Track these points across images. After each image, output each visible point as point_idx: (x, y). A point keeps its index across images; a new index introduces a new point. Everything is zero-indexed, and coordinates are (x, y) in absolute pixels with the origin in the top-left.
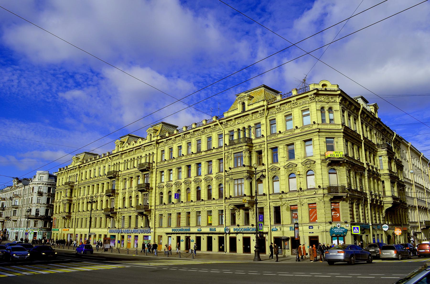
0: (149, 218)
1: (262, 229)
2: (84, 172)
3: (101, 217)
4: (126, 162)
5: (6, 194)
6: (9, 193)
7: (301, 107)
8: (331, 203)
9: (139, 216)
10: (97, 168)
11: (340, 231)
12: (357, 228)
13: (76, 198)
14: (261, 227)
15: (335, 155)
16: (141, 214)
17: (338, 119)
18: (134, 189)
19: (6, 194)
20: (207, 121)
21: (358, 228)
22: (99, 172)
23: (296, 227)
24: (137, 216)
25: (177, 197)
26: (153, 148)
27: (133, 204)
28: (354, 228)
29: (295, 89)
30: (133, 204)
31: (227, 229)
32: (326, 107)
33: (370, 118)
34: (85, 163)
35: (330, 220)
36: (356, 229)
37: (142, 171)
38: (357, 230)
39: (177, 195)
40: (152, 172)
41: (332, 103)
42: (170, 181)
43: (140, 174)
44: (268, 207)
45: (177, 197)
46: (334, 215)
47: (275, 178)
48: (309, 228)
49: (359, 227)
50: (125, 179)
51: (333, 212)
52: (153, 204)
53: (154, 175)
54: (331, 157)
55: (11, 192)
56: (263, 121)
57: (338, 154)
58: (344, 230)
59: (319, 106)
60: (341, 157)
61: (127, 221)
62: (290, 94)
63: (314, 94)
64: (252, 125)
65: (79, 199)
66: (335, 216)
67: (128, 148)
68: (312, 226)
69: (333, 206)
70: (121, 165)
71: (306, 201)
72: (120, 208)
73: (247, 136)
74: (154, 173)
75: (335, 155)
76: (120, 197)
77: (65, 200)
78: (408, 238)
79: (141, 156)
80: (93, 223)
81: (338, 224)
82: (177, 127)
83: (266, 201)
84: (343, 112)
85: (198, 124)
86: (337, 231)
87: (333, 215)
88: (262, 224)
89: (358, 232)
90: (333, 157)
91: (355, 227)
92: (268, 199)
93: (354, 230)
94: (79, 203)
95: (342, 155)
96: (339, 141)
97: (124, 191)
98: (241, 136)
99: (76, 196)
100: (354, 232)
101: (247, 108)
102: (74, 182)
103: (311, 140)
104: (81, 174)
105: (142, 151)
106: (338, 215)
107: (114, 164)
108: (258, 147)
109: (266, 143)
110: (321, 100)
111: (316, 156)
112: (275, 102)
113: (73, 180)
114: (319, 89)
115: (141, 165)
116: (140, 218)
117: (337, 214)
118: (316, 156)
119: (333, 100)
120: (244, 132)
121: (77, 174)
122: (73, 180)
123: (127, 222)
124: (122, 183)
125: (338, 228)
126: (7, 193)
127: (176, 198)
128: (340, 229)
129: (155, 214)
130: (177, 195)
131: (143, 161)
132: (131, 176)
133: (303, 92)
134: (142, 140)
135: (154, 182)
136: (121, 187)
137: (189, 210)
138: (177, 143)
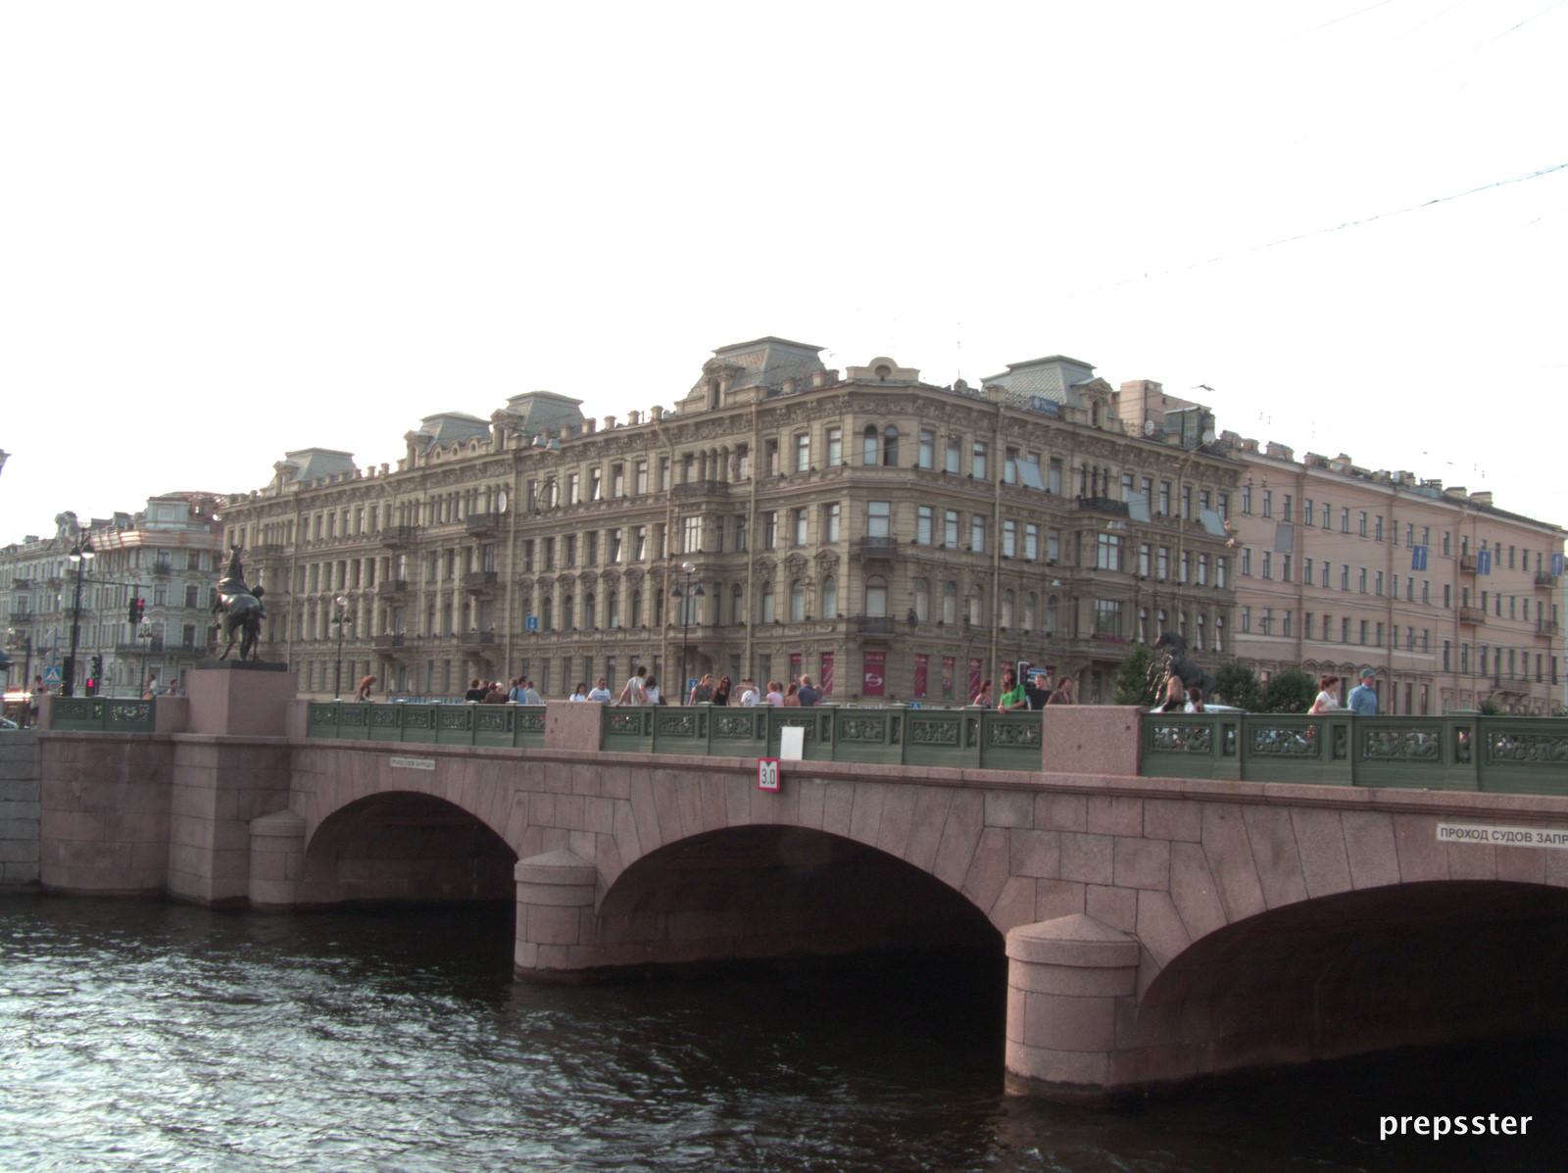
2: (312, 515)
3: (352, 659)
4: (434, 503)
5: (32, 568)
6: (43, 561)
7: (827, 420)
8: (865, 653)
10: (353, 507)
13: (290, 598)
16: (473, 656)
18: (457, 583)
19: (32, 568)
22: (358, 520)
26: (508, 470)
27: (456, 627)
30: (456, 627)
33: (127, 742)
34: (328, 487)
35: (859, 690)
37: (478, 535)
40: (505, 540)
43: (474, 543)
47: (766, 588)
50: (435, 552)
51: (868, 676)
52: (507, 631)
53: (510, 552)
55: (50, 559)
56: (752, 441)
59: (863, 422)
61: (435, 681)
63: (851, 394)
64: (731, 448)
65: (298, 603)
70: (421, 511)
71: (816, 648)
72: (419, 637)
74: (510, 543)
76: (422, 603)
77: (757, 425)
79: (476, 490)
80: (344, 677)
94: (300, 616)
97: (431, 588)
99: (291, 590)
102: (282, 547)
104: (302, 522)
106: (880, 680)
107: (403, 503)
109: (753, 499)
115: (473, 519)
119: (898, 409)
121: (290, 522)
124: (424, 563)
126: (34, 562)
131: (481, 508)
132: (448, 546)
135: (509, 569)
136: (424, 575)
138: (567, 466)
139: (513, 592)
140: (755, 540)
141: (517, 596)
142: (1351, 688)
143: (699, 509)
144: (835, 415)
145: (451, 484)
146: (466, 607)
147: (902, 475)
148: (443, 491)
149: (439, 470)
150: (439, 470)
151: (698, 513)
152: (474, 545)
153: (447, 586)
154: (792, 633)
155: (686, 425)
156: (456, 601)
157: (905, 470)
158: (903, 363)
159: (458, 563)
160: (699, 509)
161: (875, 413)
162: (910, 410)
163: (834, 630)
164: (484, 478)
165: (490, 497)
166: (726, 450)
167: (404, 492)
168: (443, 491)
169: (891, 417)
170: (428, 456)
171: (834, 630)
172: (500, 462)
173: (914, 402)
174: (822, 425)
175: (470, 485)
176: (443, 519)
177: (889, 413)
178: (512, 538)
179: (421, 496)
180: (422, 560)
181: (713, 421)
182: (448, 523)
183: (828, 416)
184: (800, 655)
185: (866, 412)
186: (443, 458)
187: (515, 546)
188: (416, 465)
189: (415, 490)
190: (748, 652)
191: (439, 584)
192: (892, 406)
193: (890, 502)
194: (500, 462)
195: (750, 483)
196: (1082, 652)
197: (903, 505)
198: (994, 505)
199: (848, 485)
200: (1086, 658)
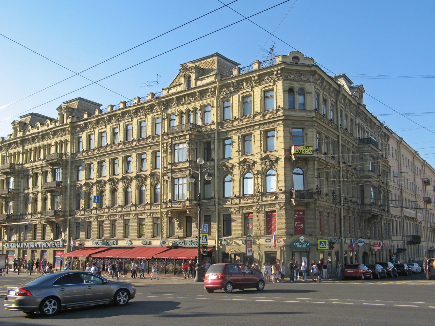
0: (413, 210)
1: (206, 242)
9: (48, 225)
11: (303, 246)
12: (324, 242)
14: (205, 239)
15: (303, 151)
17: (311, 104)
20: (141, 99)
21: (325, 242)
23: (249, 243)
24: (45, 225)
25: (96, 201)
26: (67, 133)
28: (321, 242)
29: (257, 61)
31: (163, 242)
32: (295, 87)
36: (324, 243)
37: (51, 164)
38: (324, 245)
39: (96, 198)
41: (304, 82)
42: (89, 179)
44: (217, 215)
45: (96, 201)
46: (297, 226)
48: (266, 242)
49: (327, 241)
51: (297, 223)
54: (298, 153)
57: (307, 149)
58: (308, 244)
60: (311, 153)
62: (251, 67)
63: (281, 69)
66: (298, 227)
67: (31, 132)
68: (269, 240)
69: (296, 214)
73: (191, 121)
75: (303, 151)
78: (389, 255)
81: (301, 237)
82: (101, 105)
83: (213, 207)
84: (318, 95)
85: (128, 103)
86: (300, 246)
87: (296, 225)
88: (206, 236)
89: (326, 248)
90: (300, 153)
91: (322, 241)
92: (216, 205)
93: (320, 245)
95: (311, 151)
96: (309, 133)
98: (184, 122)
100: (320, 247)
101: (193, 85)
103: (274, 130)
105: (52, 137)
108: (206, 136)
109: (216, 132)
110: (290, 78)
111: (279, 151)
112: (230, 77)
113: (410, 233)
114: (288, 63)
116: (48, 228)
117: (301, 224)
118: (279, 151)
119: (305, 79)
120: (189, 116)
122: (410, 233)
123: (94, 228)
125: (300, 242)
127: (96, 202)
128: (304, 244)
129: (70, 222)
130: (96, 198)
132: (35, 171)
133: (267, 66)
134: (51, 121)
136: (22, 186)
137: (143, 216)
138: (100, 128)
139: (70, 190)
140: (218, 153)
141: (72, 192)
142: (304, 236)
143: (185, 138)
144: (270, 82)
145: (37, 143)
146: (44, 200)
147: (309, 114)
148: (32, 146)
149: (30, 137)
150: (30, 137)
151: (184, 140)
152: (49, 170)
153: (34, 190)
154: (246, 201)
155: (172, 99)
156: (39, 196)
157: (311, 111)
158: (307, 54)
159: (40, 178)
160: (185, 138)
161: (293, 80)
162: (311, 79)
163: (277, 198)
164: (55, 137)
165: (57, 146)
166: (195, 109)
167: (12, 148)
168: (32, 146)
169: (301, 83)
170: (24, 132)
171: (277, 198)
172: (63, 130)
173: (314, 75)
174: (261, 89)
175: (46, 142)
176: (32, 159)
177: (301, 81)
178: (70, 165)
179: (20, 149)
180: (22, 178)
181: (188, 95)
182: (35, 161)
183: (266, 83)
184: (252, 213)
185: (289, 80)
186: (32, 132)
187: (71, 169)
188: (18, 136)
189: (18, 147)
190: (216, 213)
191: (31, 190)
192: (302, 77)
193: (303, 129)
194: (63, 130)
195: (214, 124)
196: (367, 210)
197: (310, 130)
198: (338, 136)
199: (283, 118)
200: (370, 213)
